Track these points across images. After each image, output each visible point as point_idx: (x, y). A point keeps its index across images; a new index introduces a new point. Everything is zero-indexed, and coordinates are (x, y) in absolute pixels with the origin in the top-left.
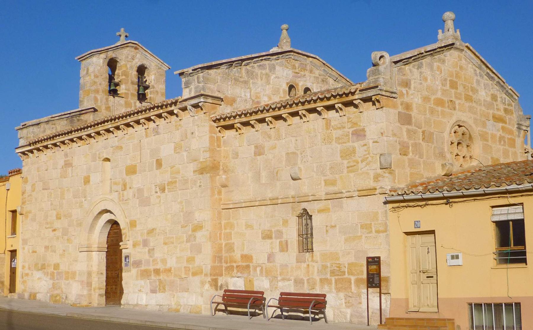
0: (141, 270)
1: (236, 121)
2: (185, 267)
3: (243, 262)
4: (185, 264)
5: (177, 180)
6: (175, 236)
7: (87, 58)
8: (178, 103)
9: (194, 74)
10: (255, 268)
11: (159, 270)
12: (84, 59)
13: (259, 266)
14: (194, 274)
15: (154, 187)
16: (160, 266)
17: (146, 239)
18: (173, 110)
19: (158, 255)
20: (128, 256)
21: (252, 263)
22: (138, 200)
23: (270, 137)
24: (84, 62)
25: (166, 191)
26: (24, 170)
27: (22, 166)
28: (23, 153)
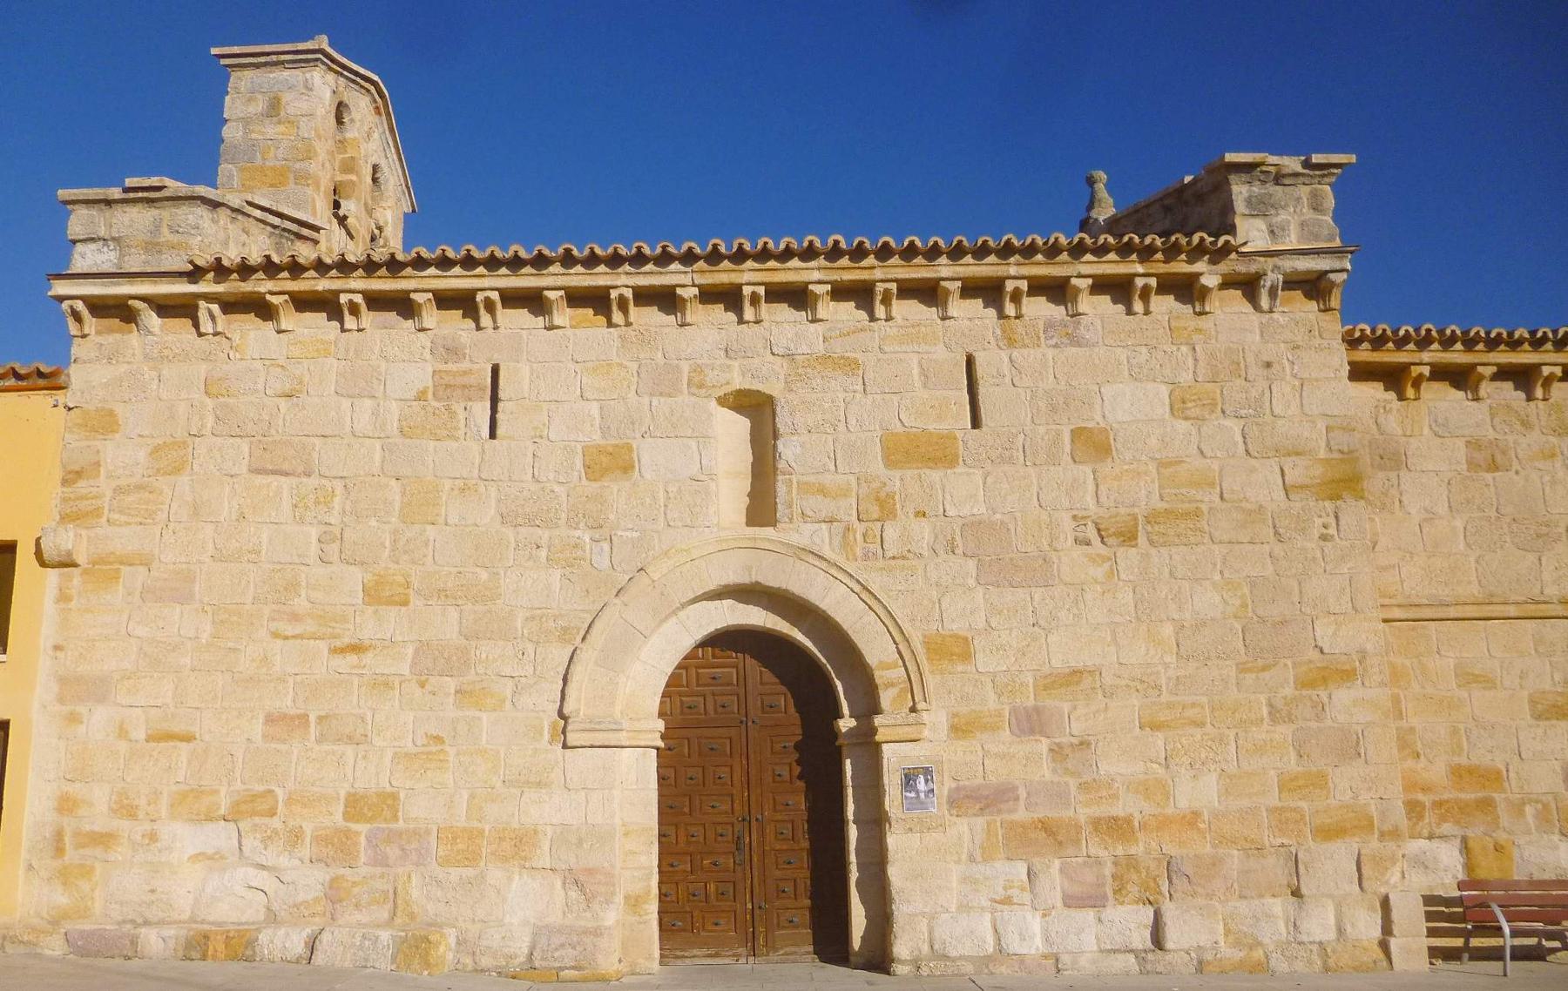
0: (1011, 826)
1: (1426, 356)
2: (1272, 811)
3: (1462, 790)
4: (1273, 800)
5: (1204, 508)
6: (1204, 699)
7: (282, 63)
8: (1233, 256)
9: (1301, 179)
10: (1518, 809)
11: (1128, 820)
12: (257, 66)
13: (1530, 801)
14: (1328, 833)
15: (1068, 524)
16: (1128, 806)
17: (1037, 709)
18: (1199, 275)
19: (1114, 766)
20: (927, 772)
21: (1504, 791)
22: (971, 565)
23: (1526, 424)
24: (248, 74)
25: (1142, 539)
26: (76, 375)
27: (66, 359)
28: (100, 307)
